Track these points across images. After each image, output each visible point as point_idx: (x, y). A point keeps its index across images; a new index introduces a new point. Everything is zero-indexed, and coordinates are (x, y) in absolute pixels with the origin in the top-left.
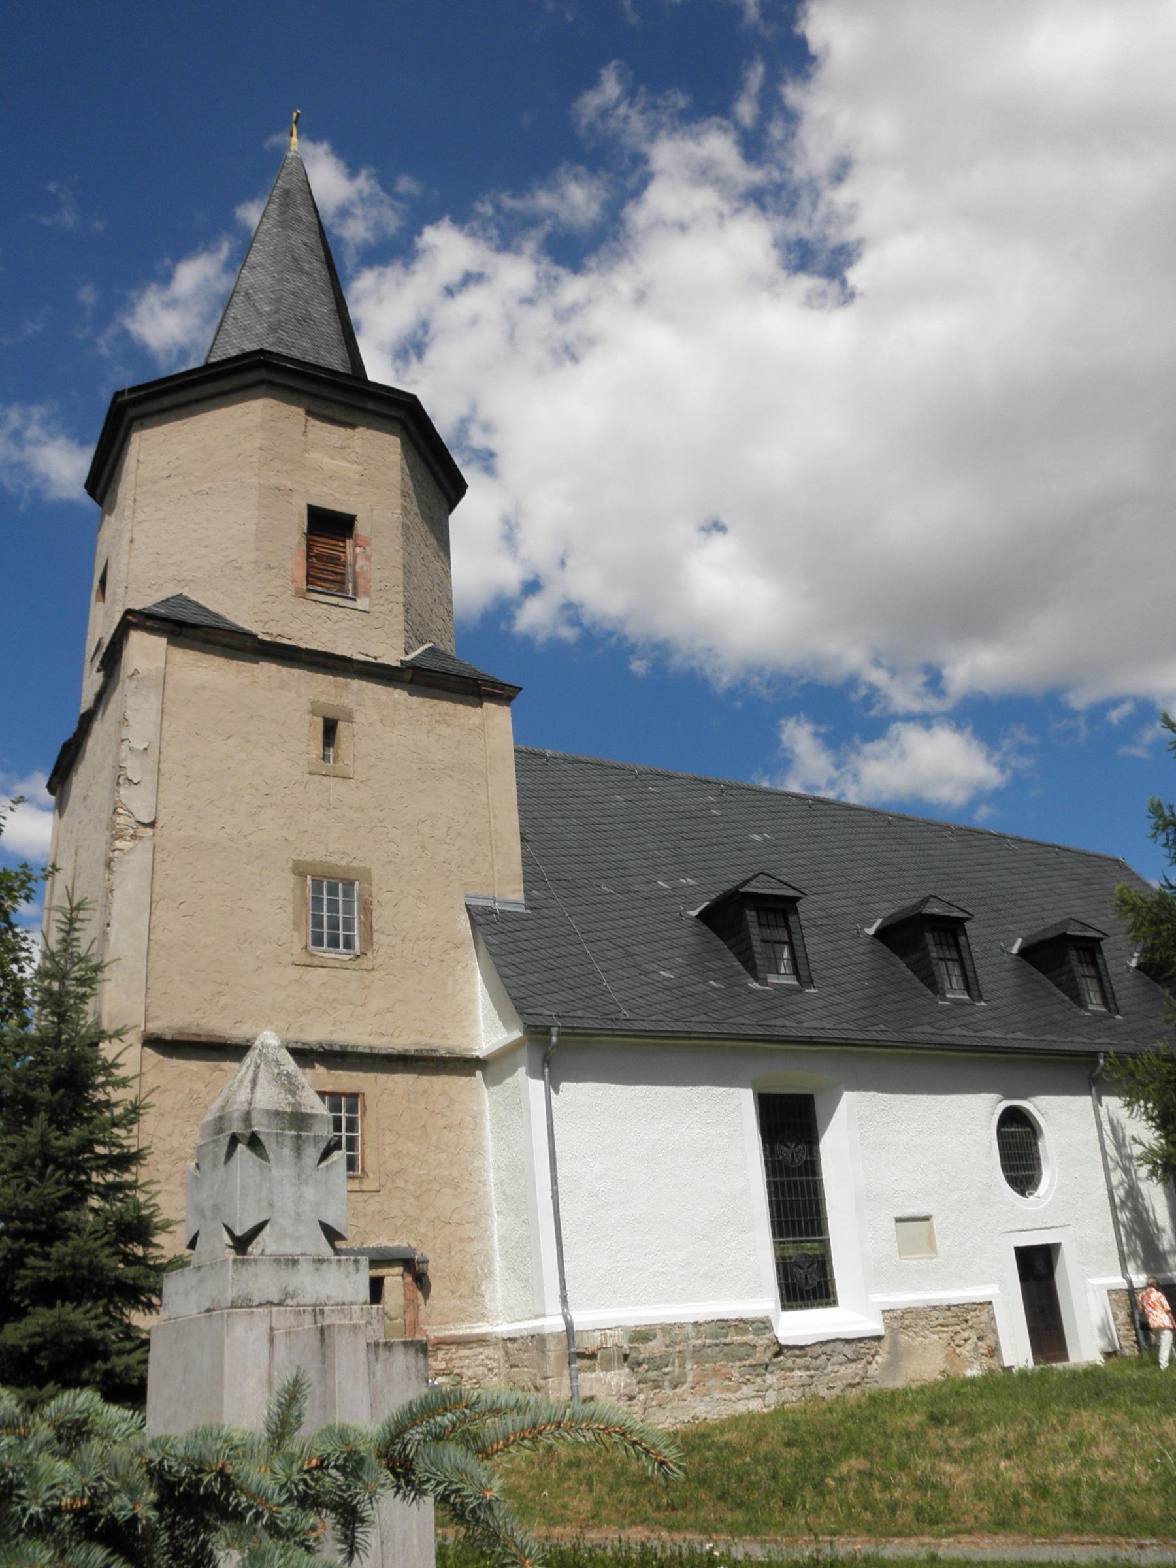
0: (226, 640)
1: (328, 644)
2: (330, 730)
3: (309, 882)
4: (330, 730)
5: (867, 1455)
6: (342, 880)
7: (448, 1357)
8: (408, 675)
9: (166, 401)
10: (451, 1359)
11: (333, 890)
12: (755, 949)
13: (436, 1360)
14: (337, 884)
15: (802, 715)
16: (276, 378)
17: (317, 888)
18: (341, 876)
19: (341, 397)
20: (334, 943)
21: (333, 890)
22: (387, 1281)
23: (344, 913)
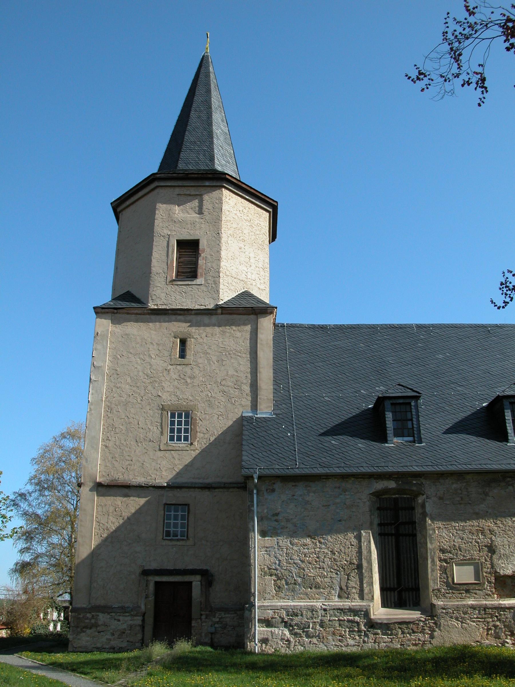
0: (136, 311)
1: (184, 304)
2: (183, 342)
3: (169, 414)
4: (183, 342)
5: (453, 554)
6: (184, 411)
7: (220, 616)
8: (219, 311)
9: (128, 203)
10: (222, 618)
11: (180, 416)
12: (387, 426)
13: (215, 617)
14: (182, 414)
15: (214, 671)
16: (162, 184)
17: (173, 416)
18: (184, 409)
19: (192, 184)
20: (179, 439)
21: (180, 416)
22: (194, 583)
23: (174, 436)
